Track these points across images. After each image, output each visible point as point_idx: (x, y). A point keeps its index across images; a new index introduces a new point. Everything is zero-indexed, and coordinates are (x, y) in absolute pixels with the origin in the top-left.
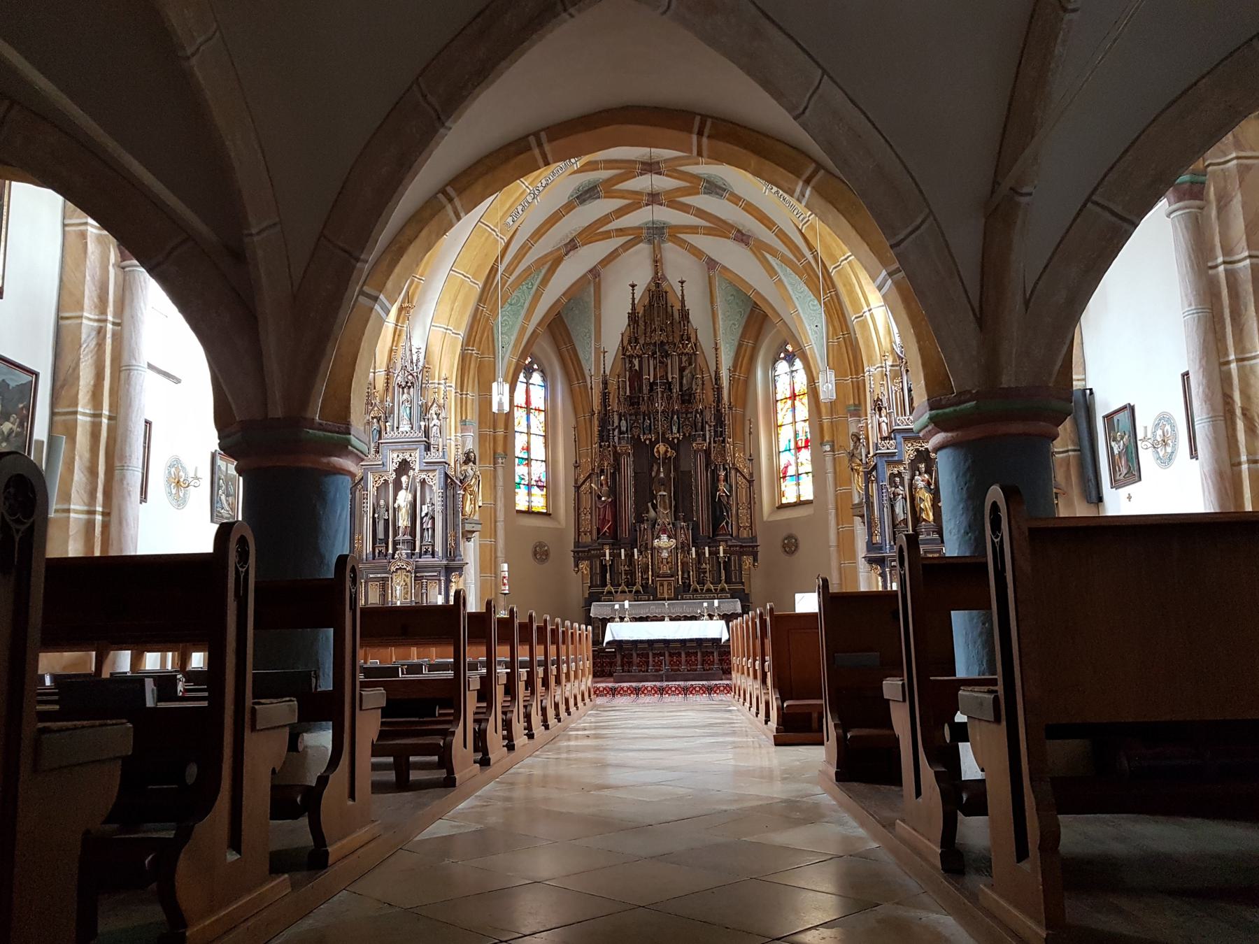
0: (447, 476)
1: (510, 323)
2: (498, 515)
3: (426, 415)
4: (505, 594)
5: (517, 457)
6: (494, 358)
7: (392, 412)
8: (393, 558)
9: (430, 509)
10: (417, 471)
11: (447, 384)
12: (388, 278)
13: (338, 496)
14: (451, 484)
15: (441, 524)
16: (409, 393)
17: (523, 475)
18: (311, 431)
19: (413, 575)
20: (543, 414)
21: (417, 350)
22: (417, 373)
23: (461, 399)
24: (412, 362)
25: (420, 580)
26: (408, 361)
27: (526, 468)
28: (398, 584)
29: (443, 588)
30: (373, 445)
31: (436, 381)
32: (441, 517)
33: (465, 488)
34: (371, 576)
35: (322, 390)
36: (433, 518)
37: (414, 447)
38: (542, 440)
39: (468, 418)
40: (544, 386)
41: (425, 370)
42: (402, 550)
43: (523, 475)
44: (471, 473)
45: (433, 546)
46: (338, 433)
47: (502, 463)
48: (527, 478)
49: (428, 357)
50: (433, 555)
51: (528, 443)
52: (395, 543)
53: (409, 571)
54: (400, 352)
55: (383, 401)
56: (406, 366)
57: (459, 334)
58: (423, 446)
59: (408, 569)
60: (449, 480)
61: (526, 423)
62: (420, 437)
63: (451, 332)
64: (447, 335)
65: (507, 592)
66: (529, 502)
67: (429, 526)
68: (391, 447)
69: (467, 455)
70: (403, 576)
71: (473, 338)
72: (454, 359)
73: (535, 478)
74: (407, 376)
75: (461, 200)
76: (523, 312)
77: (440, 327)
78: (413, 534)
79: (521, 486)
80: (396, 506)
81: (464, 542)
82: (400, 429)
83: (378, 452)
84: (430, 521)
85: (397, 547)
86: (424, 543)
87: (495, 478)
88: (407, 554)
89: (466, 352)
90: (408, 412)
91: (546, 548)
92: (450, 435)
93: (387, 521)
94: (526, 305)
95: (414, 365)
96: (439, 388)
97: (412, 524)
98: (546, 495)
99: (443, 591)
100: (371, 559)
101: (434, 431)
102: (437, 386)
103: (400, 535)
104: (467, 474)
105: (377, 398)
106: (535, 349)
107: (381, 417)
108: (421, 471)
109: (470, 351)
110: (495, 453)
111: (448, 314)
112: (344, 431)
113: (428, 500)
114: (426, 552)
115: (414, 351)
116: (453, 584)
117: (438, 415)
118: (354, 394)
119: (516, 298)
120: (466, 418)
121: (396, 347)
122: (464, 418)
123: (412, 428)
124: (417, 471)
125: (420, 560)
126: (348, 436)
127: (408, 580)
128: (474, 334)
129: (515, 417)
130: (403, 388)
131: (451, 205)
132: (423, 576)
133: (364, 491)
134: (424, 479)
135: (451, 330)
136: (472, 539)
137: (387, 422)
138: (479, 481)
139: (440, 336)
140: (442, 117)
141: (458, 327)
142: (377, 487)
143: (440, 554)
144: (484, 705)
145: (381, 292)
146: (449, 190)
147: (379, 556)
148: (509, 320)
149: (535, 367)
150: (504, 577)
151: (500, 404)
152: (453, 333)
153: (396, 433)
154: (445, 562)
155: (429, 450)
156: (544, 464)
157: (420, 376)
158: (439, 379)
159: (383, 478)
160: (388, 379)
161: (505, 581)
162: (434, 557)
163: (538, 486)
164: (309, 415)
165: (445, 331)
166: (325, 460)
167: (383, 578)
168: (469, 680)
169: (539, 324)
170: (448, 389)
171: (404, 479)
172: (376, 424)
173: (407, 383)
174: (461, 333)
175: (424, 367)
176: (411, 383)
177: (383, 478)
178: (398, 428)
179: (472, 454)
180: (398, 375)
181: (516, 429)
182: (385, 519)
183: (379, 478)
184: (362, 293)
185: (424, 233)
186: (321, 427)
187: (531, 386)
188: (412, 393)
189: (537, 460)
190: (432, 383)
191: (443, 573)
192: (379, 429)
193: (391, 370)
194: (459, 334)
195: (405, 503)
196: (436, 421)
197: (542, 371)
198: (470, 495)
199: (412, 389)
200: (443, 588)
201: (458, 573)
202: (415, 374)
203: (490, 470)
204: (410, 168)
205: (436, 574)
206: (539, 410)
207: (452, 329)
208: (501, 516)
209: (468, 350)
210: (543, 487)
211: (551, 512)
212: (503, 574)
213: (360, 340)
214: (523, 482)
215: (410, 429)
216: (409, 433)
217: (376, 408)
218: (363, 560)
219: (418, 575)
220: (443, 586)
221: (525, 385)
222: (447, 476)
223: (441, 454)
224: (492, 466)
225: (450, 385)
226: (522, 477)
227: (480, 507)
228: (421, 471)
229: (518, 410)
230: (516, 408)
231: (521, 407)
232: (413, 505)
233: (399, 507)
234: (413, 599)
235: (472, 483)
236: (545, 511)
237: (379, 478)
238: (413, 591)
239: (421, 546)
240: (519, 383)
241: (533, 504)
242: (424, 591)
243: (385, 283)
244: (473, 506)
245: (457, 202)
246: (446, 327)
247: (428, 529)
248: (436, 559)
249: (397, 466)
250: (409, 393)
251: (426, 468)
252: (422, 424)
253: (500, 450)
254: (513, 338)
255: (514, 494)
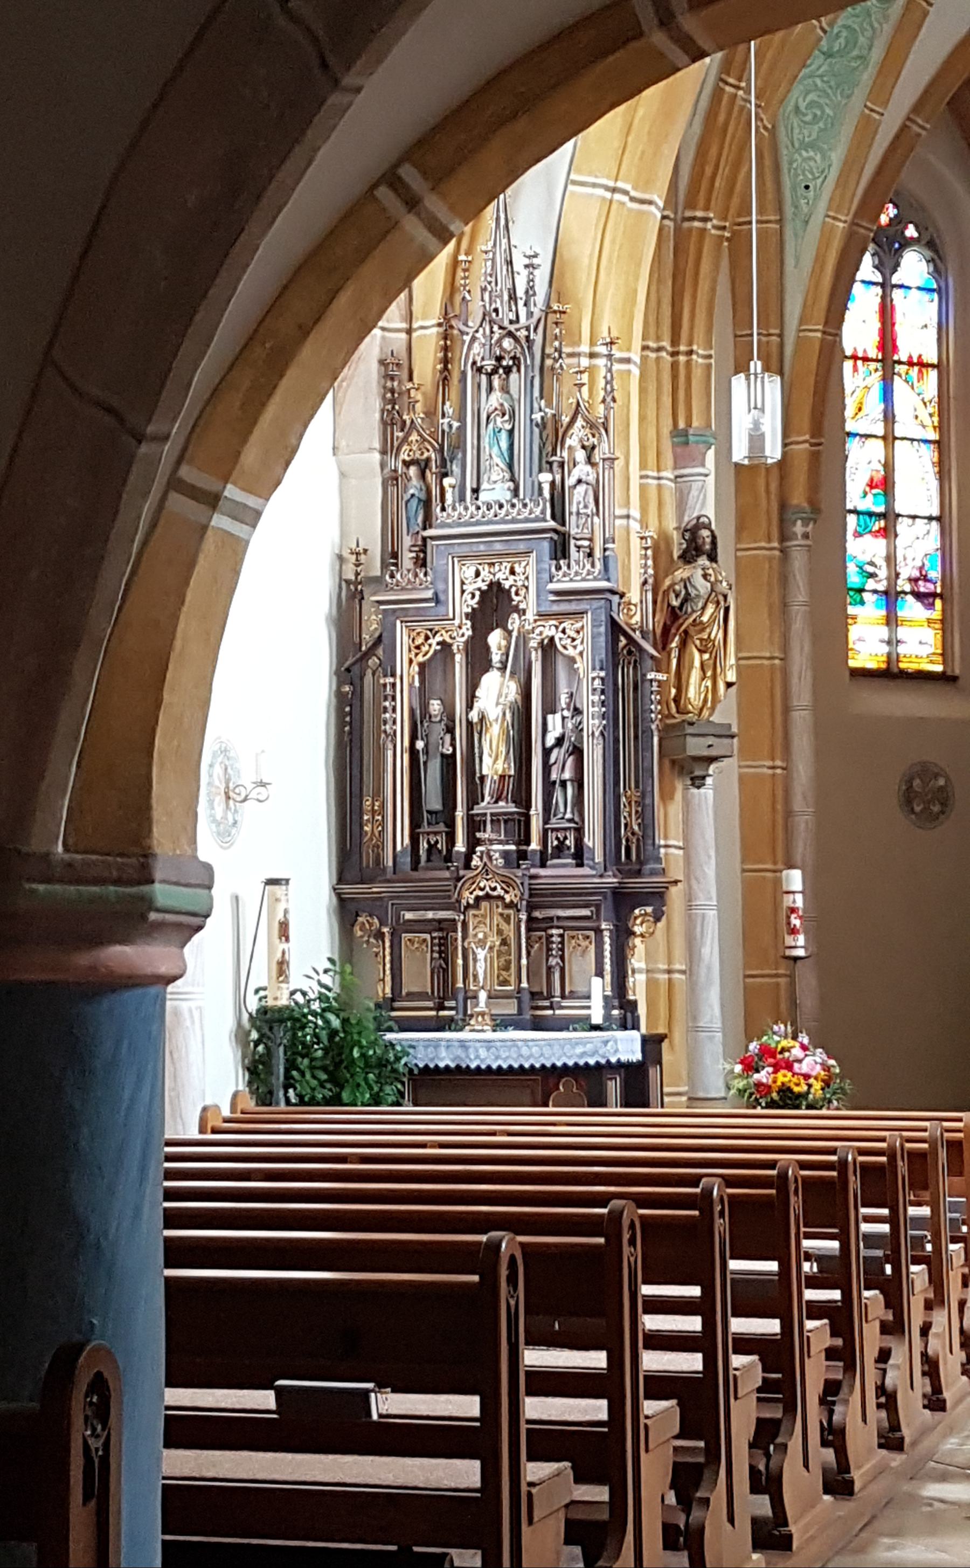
0: (615, 629)
1: (828, 111)
2: (795, 689)
3: (554, 453)
4: (796, 959)
5: (855, 511)
6: (780, 221)
7: (460, 444)
8: (467, 866)
9: (570, 725)
10: (530, 615)
11: (618, 354)
12: (244, 440)
13: (124, 1050)
14: (630, 653)
15: (599, 771)
16: (505, 390)
17: (872, 564)
18: (41, 887)
19: (524, 917)
20: (933, 375)
21: (527, 261)
22: (528, 329)
23: (674, 366)
24: (513, 297)
25: (545, 930)
26: (501, 296)
27: (882, 543)
28: (482, 943)
29: (607, 954)
30: (407, 541)
31: (585, 348)
32: (599, 751)
33: (686, 632)
34: (409, 916)
35: (67, 778)
36: (577, 752)
37: (522, 547)
38: (928, 455)
39: (695, 424)
40: (939, 290)
41: (552, 318)
42: (491, 842)
43: (872, 564)
44: (702, 586)
45: (579, 831)
46: (117, 882)
47: (806, 536)
48: (883, 573)
49: (562, 274)
50: (579, 856)
51: (889, 466)
52: (474, 824)
53: (511, 905)
54: (481, 268)
55: (435, 413)
56: (496, 310)
57: (650, 203)
58: (546, 545)
59: (508, 898)
60: (623, 641)
61: (882, 406)
62: (536, 520)
63: (625, 199)
64: (614, 206)
65: (801, 953)
66: (889, 643)
67: (567, 775)
68: (457, 549)
69: (692, 533)
70: (497, 919)
71: (705, 184)
72: (637, 279)
73: (907, 571)
74: (499, 341)
75: (443, 196)
76: (867, 77)
77: (594, 185)
78: (523, 799)
79: (866, 596)
80: (474, 716)
81: (686, 789)
82: (484, 496)
83: (424, 565)
84: (570, 761)
85: (478, 835)
86: (554, 823)
87: (784, 579)
88: (505, 855)
89: (686, 225)
90: (504, 444)
91: (941, 782)
92: (627, 504)
93: (449, 761)
94: (876, 55)
95: (521, 303)
96: (591, 370)
97: (519, 769)
98: (942, 621)
99: (607, 961)
100: (408, 867)
101: (578, 498)
102: (585, 362)
103: (487, 798)
104: (693, 592)
105: (419, 407)
106: (909, 179)
107: (428, 460)
108: (542, 616)
109: (697, 224)
110: (783, 506)
111: (617, 144)
112: (135, 876)
113: (563, 699)
114: (560, 849)
115: (519, 262)
116: (638, 941)
117: (590, 451)
118: (162, 766)
119: (844, 34)
120: (689, 424)
121: (467, 254)
122: (682, 425)
123: (516, 492)
124: (530, 615)
125: (542, 872)
126: (145, 889)
127: (510, 931)
128: (709, 170)
129: (848, 391)
130: (490, 375)
131: (418, 215)
132: (551, 919)
133: (385, 676)
134: (552, 639)
135: (626, 193)
136: (709, 781)
137: (445, 475)
138: (727, 610)
139: (594, 212)
140: (331, 60)
141: (645, 183)
142: (422, 666)
143: (599, 858)
144: (601, 1493)
145: (226, 482)
146: (408, 173)
147: (429, 860)
148: (822, 101)
149: (911, 232)
150: (793, 910)
151: (756, 440)
152: (632, 199)
153: (472, 509)
154: (611, 880)
155: (565, 554)
156: (935, 525)
157: (538, 338)
158: (592, 343)
159: (438, 638)
160: (446, 349)
161: (796, 922)
162: (580, 865)
163: (918, 596)
164: (36, 845)
165: (608, 195)
166: (84, 959)
167: (440, 921)
168: (530, 1495)
169: (917, 108)
170: (617, 367)
171: (495, 639)
172: (415, 482)
173: (499, 359)
174: (655, 198)
175: (548, 310)
176: (514, 358)
177: (438, 638)
178: (476, 491)
179: (705, 533)
180: (474, 339)
181: (850, 426)
182: (443, 755)
183: (427, 638)
184: (175, 484)
185: (343, 299)
186: (72, 874)
187: (897, 295)
188: (514, 390)
189: (914, 517)
190: (571, 355)
191: (606, 909)
192: (423, 496)
193: (454, 323)
194: (650, 203)
195: (499, 710)
196: (582, 470)
197: (931, 245)
198: (701, 652)
199: (514, 376)
200: (607, 954)
201: (649, 909)
202: (522, 334)
203: (770, 559)
204: (259, 197)
205: (585, 912)
206: (922, 365)
207: (628, 187)
208: (802, 694)
209: (693, 219)
210: (934, 595)
211: (957, 672)
212: (788, 901)
213: (175, 618)
214: (871, 584)
215: (508, 495)
216: (507, 507)
217: (414, 437)
218: (384, 869)
219: (537, 914)
220: (607, 947)
221: (879, 290)
222: (615, 629)
223: (599, 565)
224: (776, 544)
225: (625, 355)
226: (870, 569)
227: (729, 685)
228: (542, 616)
229: (855, 369)
230: (848, 365)
231: (866, 359)
232: (522, 712)
233: (482, 719)
234: (524, 985)
235: (705, 619)
236: (939, 668)
237: (427, 638)
238: (524, 961)
239: (545, 832)
240: (857, 288)
241: (901, 649)
242: (553, 961)
243: (238, 454)
244: (709, 684)
245: (433, 204)
246: (611, 184)
247: (563, 784)
248: (585, 871)
249: (474, 603)
250: (505, 390)
251: (556, 608)
252: (546, 477)
253: (798, 498)
254: (837, 157)
255: (844, 622)
